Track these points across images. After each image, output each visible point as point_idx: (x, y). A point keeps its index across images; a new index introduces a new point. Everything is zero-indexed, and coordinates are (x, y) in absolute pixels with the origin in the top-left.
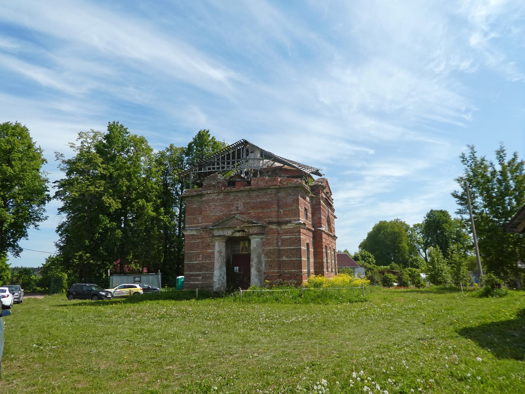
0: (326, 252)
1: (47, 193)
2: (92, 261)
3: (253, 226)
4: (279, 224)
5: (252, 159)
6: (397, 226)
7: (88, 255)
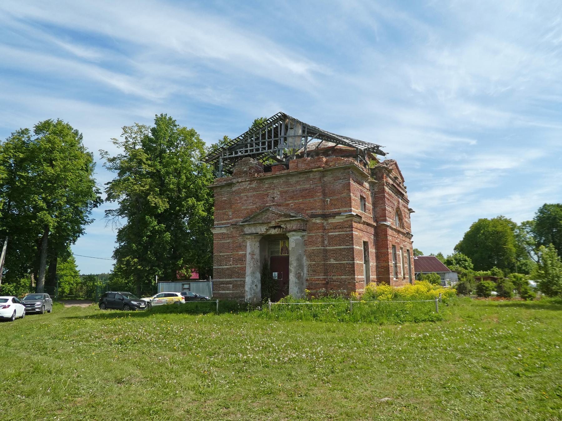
0: (395, 254)
1: (98, 195)
2: (139, 267)
3: (293, 220)
4: (325, 216)
5: (292, 136)
6: (501, 224)
7: (136, 260)
